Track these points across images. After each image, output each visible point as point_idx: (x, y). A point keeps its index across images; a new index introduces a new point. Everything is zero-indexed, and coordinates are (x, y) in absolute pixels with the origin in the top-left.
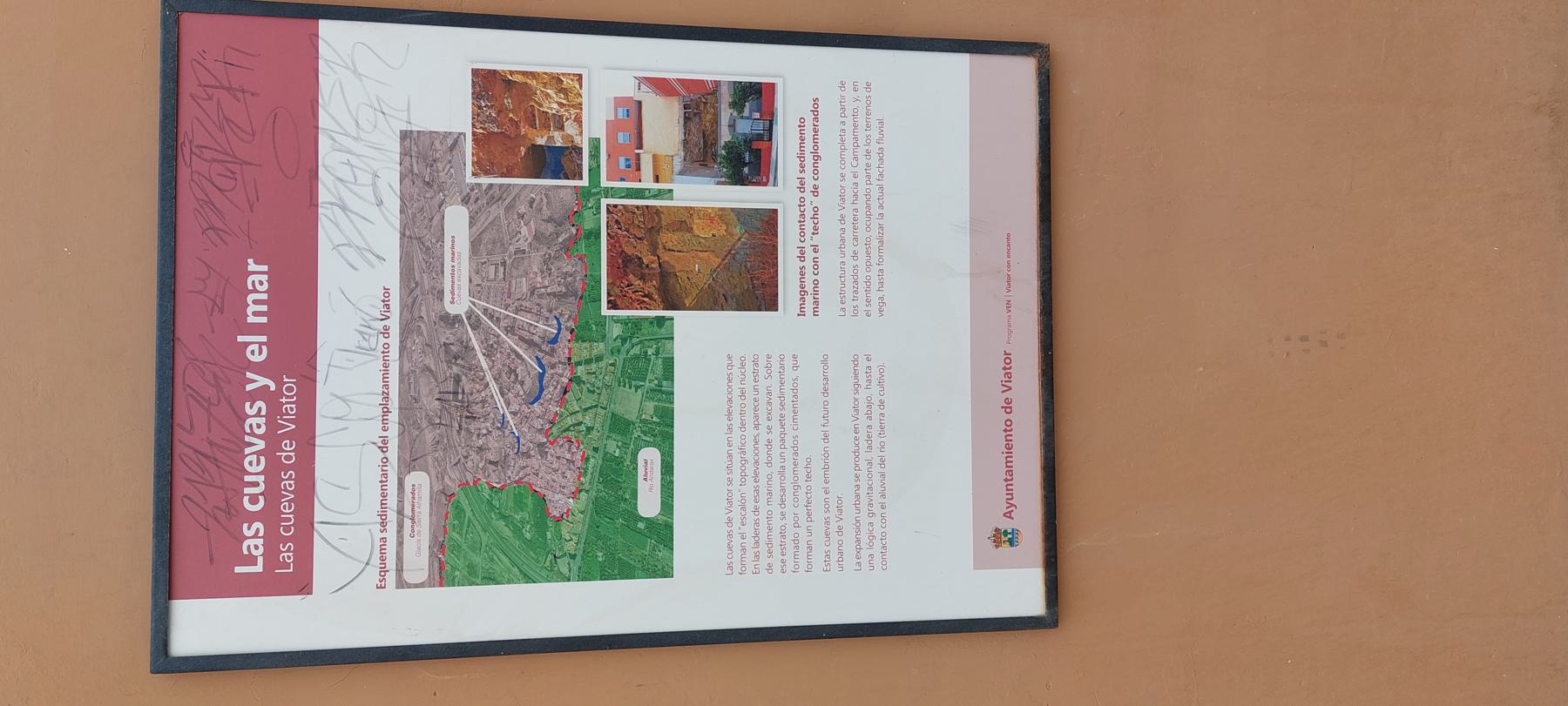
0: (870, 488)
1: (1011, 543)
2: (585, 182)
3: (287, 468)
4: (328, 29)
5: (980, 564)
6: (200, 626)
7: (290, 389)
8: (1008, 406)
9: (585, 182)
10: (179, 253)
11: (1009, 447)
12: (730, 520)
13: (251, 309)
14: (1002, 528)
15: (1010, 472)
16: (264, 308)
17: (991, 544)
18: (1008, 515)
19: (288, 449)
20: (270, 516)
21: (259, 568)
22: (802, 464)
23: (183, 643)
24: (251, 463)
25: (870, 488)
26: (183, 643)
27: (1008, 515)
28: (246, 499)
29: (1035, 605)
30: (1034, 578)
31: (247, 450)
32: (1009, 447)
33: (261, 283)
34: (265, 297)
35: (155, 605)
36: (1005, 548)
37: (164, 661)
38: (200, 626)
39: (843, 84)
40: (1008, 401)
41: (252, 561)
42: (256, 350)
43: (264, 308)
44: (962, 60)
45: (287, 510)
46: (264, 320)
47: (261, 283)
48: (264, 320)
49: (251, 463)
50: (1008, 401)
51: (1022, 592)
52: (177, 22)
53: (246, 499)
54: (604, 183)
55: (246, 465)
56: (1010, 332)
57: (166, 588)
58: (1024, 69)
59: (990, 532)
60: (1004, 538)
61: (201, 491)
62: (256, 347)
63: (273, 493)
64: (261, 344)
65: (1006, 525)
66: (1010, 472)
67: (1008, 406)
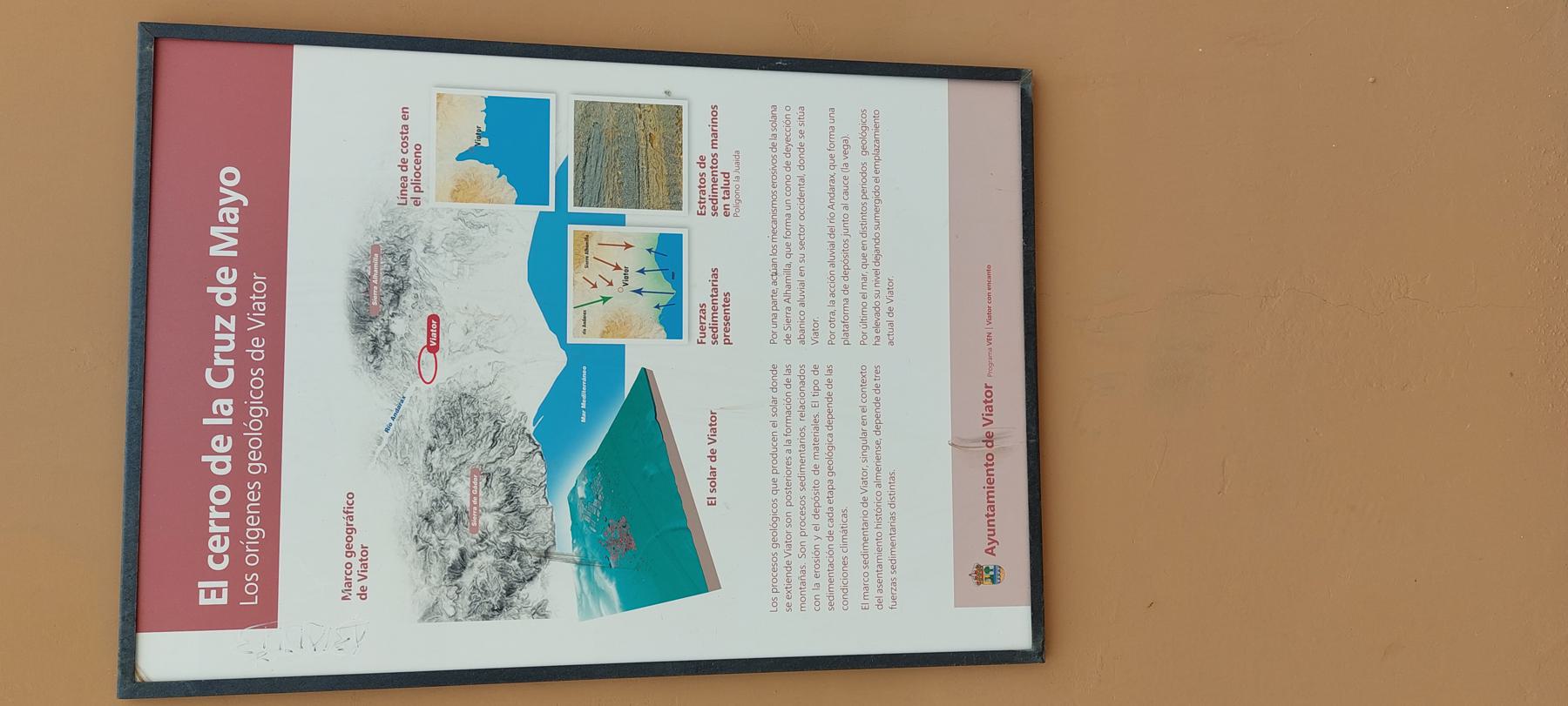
0: (831, 564)
1: (993, 579)
2: (551, 208)
3: (256, 365)
7: (260, 287)
9: (551, 208)
10: (151, 281)
11: (990, 482)
12: (774, 146)
13: (214, 514)
14: (984, 564)
15: (991, 507)
16: (226, 515)
18: (990, 551)
19: (258, 346)
21: (224, 601)
24: (215, 544)
25: (831, 564)
27: (990, 551)
28: (210, 558)
30: (1024, 613)
31: (222, 202)
32: (990, 482)
33: (226, 407)
34: (235, 230)
35: (123, 632)
36: (987, 585)
38: (167, 655)
40: (713, 452)
41: (252, 598)
43: (226, 515)
44: (938, 89)
45: (255, 434)
46: (234, 253)
47: (232, 216)
48: (234, 253)
49: (215, 544)
51: (1009, 626)
53: (210, 558)
54: (571, 208)
55: (218, 276)
56: (991, 364)
57: (132, 624)
58: (1006, 98)
60: (986, 575)
61: (172, 503)
64: (223, 535)
66: (991, 507)
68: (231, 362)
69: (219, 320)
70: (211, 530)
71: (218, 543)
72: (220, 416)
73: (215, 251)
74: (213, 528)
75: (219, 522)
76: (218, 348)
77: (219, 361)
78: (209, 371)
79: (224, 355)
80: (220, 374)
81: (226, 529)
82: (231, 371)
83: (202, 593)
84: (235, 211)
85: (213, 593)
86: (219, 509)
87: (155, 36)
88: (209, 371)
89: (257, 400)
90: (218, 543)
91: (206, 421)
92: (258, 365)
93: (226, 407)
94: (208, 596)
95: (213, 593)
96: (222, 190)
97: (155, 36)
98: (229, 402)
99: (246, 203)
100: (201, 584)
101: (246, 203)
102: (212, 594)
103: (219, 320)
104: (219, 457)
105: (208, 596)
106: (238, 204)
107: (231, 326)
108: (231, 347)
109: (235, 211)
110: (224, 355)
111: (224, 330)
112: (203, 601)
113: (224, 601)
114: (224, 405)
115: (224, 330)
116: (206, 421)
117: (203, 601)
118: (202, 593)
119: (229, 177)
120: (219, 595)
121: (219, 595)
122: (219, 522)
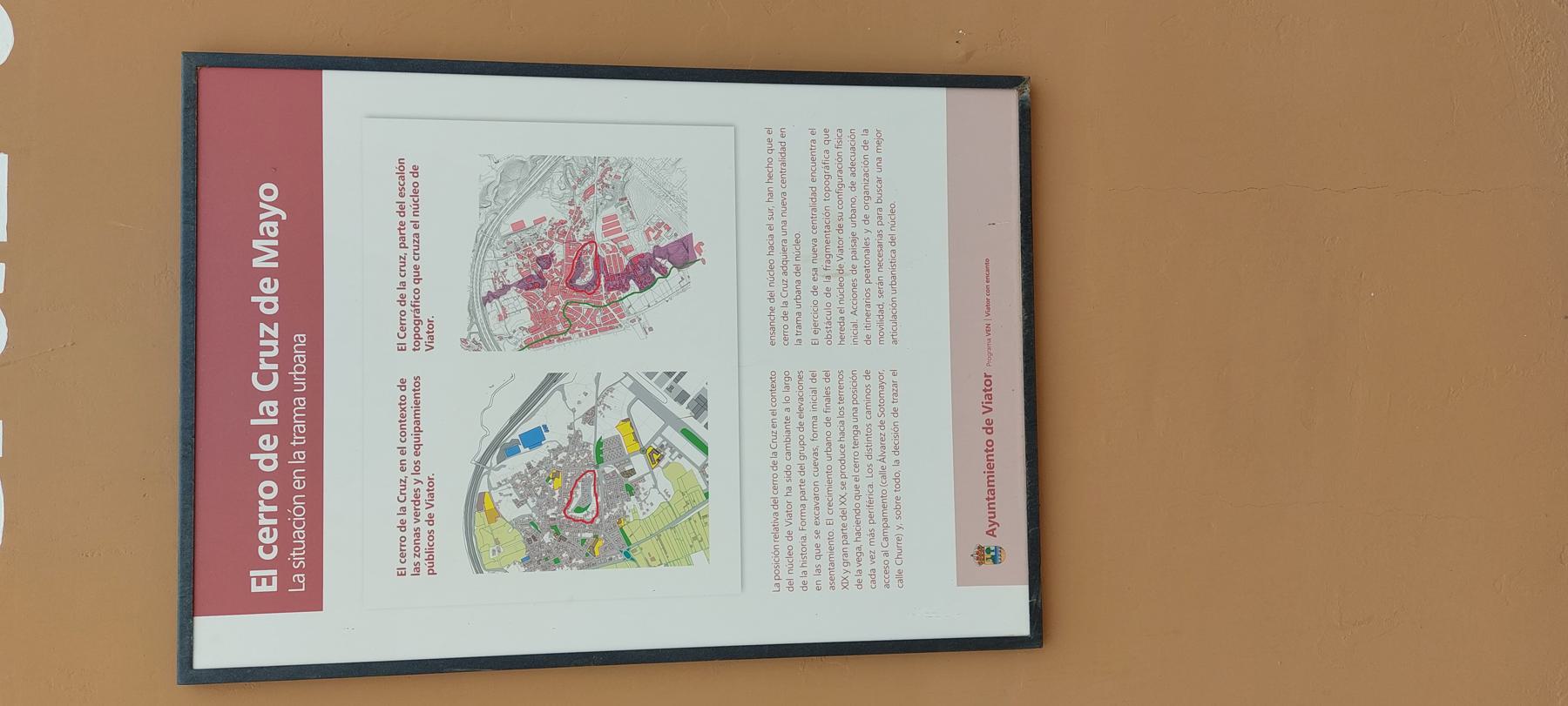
0: (866, 174)
4: (326, 73)
5: (961, 582)
6: (223, 641)
8: (989, 427)
10: (198, 526)
11: (990, 467)
13: (263, 508)
14: (985, 545)
15: (991, 491)
16: (274, 508)
17: (974, 562)
18: (991, 533)
20: (284, 394)
21: (274, 588)
22: (791, 240)
23: (204, 659)
25: (866, 174)
26: (204, 659)
27: (991, 533)
28: (261, 548)
29: (1021, 626)
31: (262, 217)
32: (990, 467)
33: (272, 409)
36: (989, 565)
37: (189, 675)
38: (223, 641)
39: (403, 381)
40: (989, 422)
42: (268, 297)
43: (274, 508)
44: (939, 95)
46: (275, 265)
48: (275, 265)
50: (989, 422)
51: (1007, 611)
52: (197, 74)
53: (261, 548)
57: (188, 611)
59: (974, 550)
60: (987, 555)
62: (267, 530)
63: (286, 542)
64: (272, 527)
65: (989, 542)
66: (991, 491)
67: (989, 427)
68: (275, 366)
69: (263, 328)
70: (261, 523)
71: (267, 536)
72: (266, 416)
73: (257, 263)
74: (263, 521)
75: (268, 515)
76: (262, 354)
77: (264, 366)
78: (255, 375)
79: (268, 360)
80: (265, 377)
81: (274, 522)
82: (275, 375)
83: (254, 581)
84: (275, 224)
85: (264, 581)
86: (267, 503)
87: (196, 63)
88: (255, 375)
89: (299, 531)
90: (267, 536)
91: (254, 422)
92: (268, 476)
93: (272, 409)
94: (259, 583)
95: (264, 581)
96: (262, 205)
97: (196, 63)
98: (275, 404)
99: (284, 217)
100: (252, 573)
101: (284, 217)
102: (263, 582)
103: (263, 328)
104: (266, 455)
105: (259, 583)
106: (276, 218)
107: (275, 333)
108: (275, 353)
109: (275, 224)
110: (268, 360)
111: (268, 337)
112: (255, 589)
113: (274, 588)
114: (270, 407)
115: (268, 337)
116: (254, 422)
117: (255, 589)
118: (254, 581)
119: (268, 192)
120: (269, 583)
121: (269, 583)
122: (268, 515)
